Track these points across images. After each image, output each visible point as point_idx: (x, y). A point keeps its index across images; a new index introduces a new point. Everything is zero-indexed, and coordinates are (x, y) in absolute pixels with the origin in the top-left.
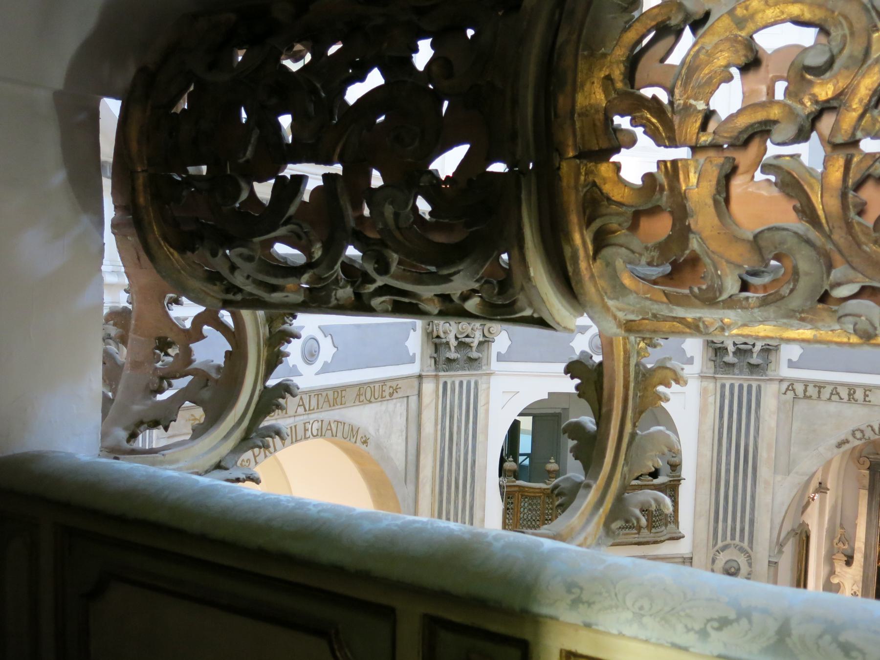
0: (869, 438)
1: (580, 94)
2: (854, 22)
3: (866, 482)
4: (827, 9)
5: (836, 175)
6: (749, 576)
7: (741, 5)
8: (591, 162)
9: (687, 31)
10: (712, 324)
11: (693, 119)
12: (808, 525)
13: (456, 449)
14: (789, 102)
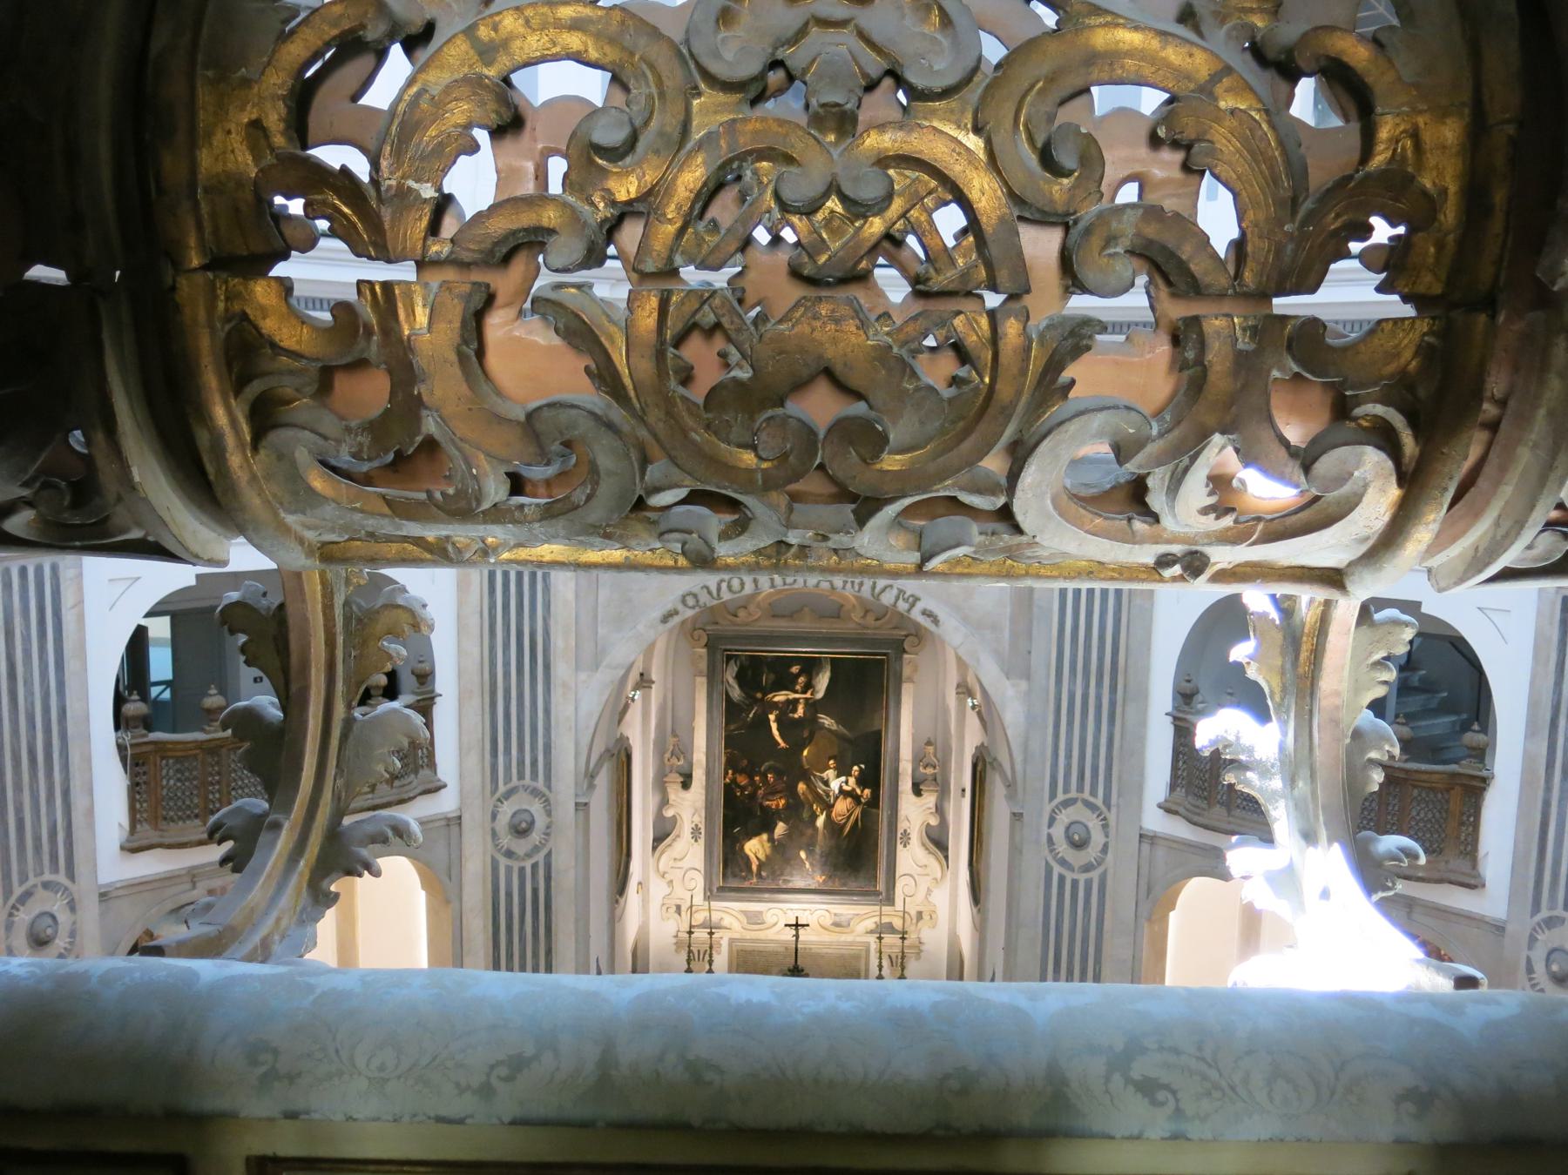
0: (705, 604)
1: (204, 151)
2: (664, 74)
3: (703, 665)
4: (624, 49)
5: (647, 320)
7: (485, 22)
8: (235, 275)
9: (396, 50)
10: (468, 545)
11: (415, 214)
12: (628, 738)
13: (25, 691)
14: (571, 199)
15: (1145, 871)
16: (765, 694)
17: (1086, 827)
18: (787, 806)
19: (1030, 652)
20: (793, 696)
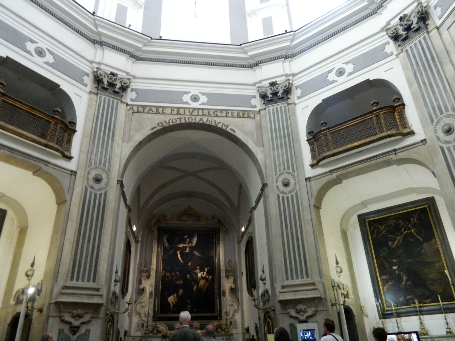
6: (107, 184)
15: (309, 190)
16: (176, 245)
17: (288, 179)
19: (263, 140)
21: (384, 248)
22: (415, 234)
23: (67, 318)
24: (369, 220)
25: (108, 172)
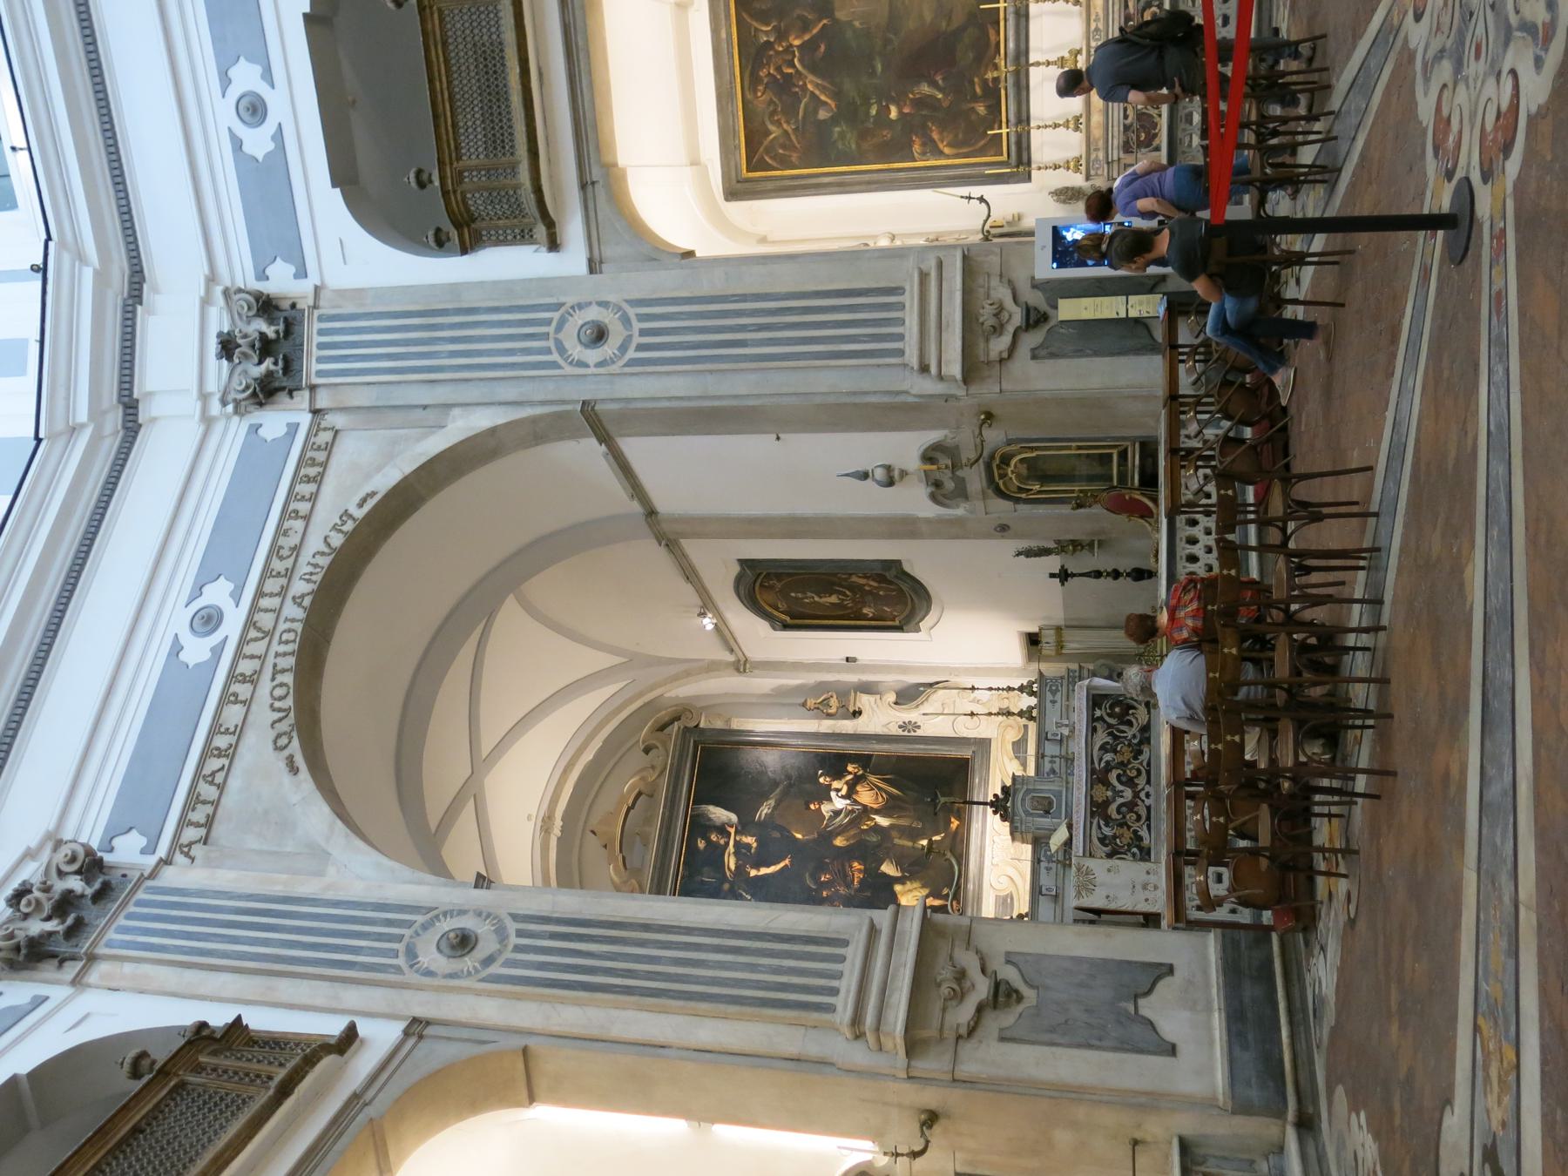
17: (582, 327)
18: (862, 860)
20: (731, 848)
21: (836, 135)
22: (807, 37)
23: (964, 1014)
24: (744, 167)
25: (435, 912)
